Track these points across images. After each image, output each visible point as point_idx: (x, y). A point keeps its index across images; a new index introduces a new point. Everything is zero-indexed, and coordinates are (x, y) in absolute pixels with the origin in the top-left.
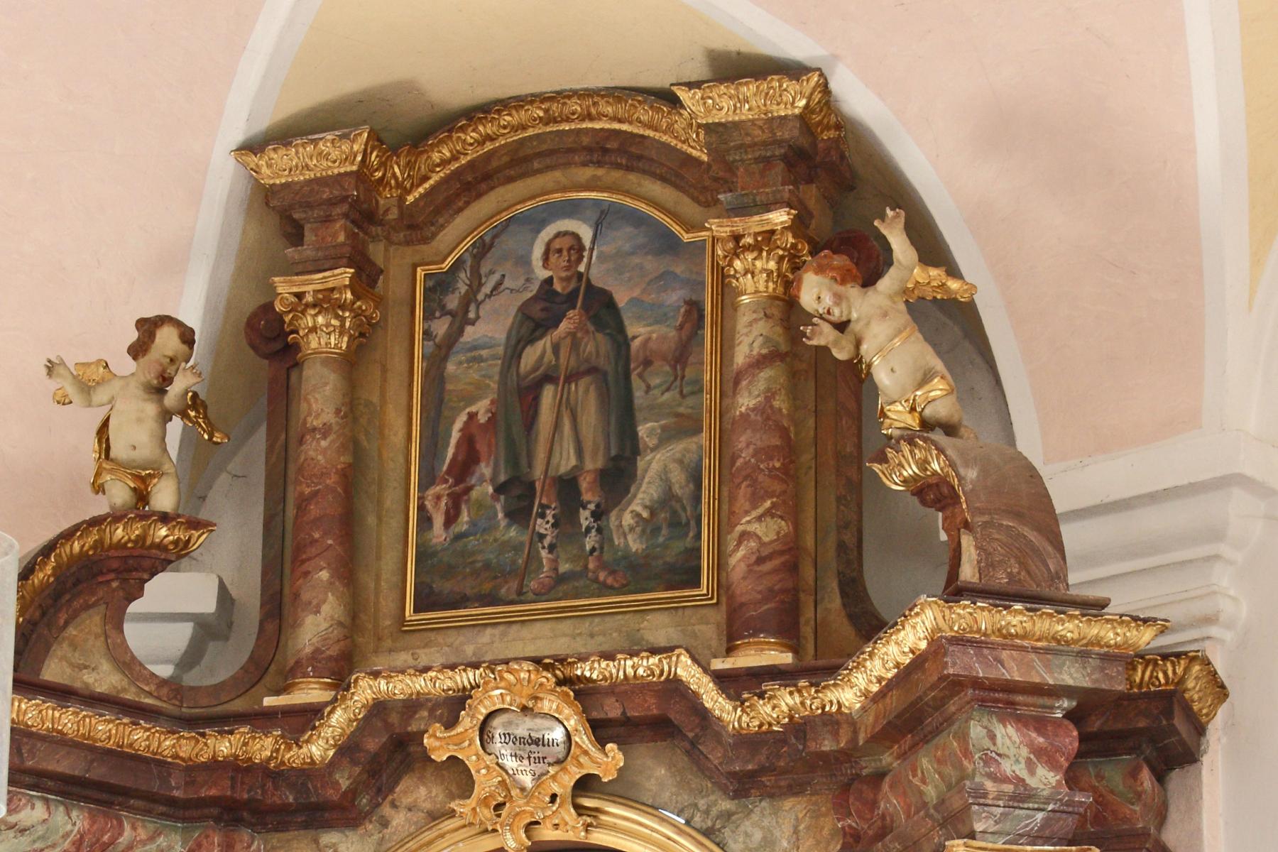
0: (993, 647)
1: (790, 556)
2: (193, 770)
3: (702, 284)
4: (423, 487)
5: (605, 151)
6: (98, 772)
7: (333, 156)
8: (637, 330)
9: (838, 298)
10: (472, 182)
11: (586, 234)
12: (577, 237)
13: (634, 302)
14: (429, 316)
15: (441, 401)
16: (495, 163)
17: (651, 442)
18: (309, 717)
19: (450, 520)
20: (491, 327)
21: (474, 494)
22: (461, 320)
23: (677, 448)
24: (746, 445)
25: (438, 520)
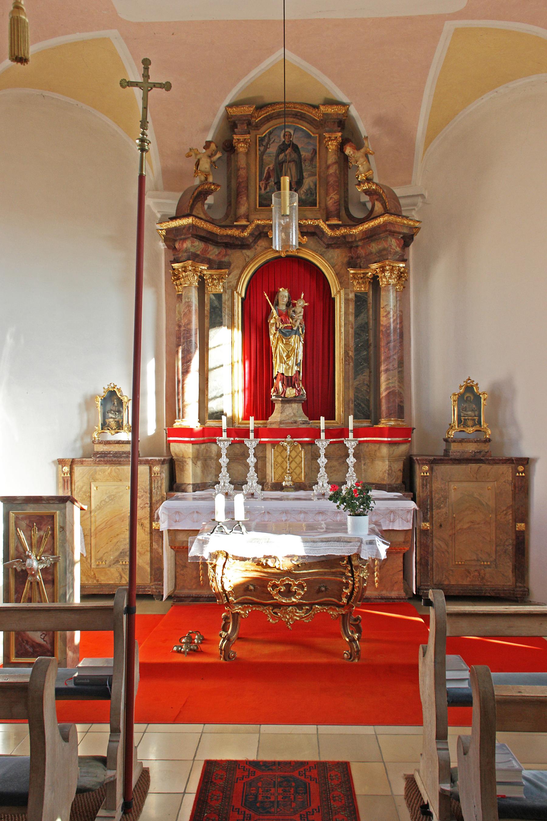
0: (394, 224)
1: (338, 203)
2: (223, 236)
3: (316, 146)
4: (259, 182)
5: (296, 115)
6: (208, 236)
7: (248, 110)
8: (303, 154)
9: (354, 153)
10: (269, 119)
11: (292, 133)
12: (290, 133)
13: (302, 147)
14: (260, 146)
15: (262, 164)
16: (274, 115)
17: (306, 177)
18: (244, 228)
19: (265, 189)
20: (273, 149)
21: (270, 184)
22: (266, 148)
23: (312, 178)
24: (332, 180)
25: (263, 189)
